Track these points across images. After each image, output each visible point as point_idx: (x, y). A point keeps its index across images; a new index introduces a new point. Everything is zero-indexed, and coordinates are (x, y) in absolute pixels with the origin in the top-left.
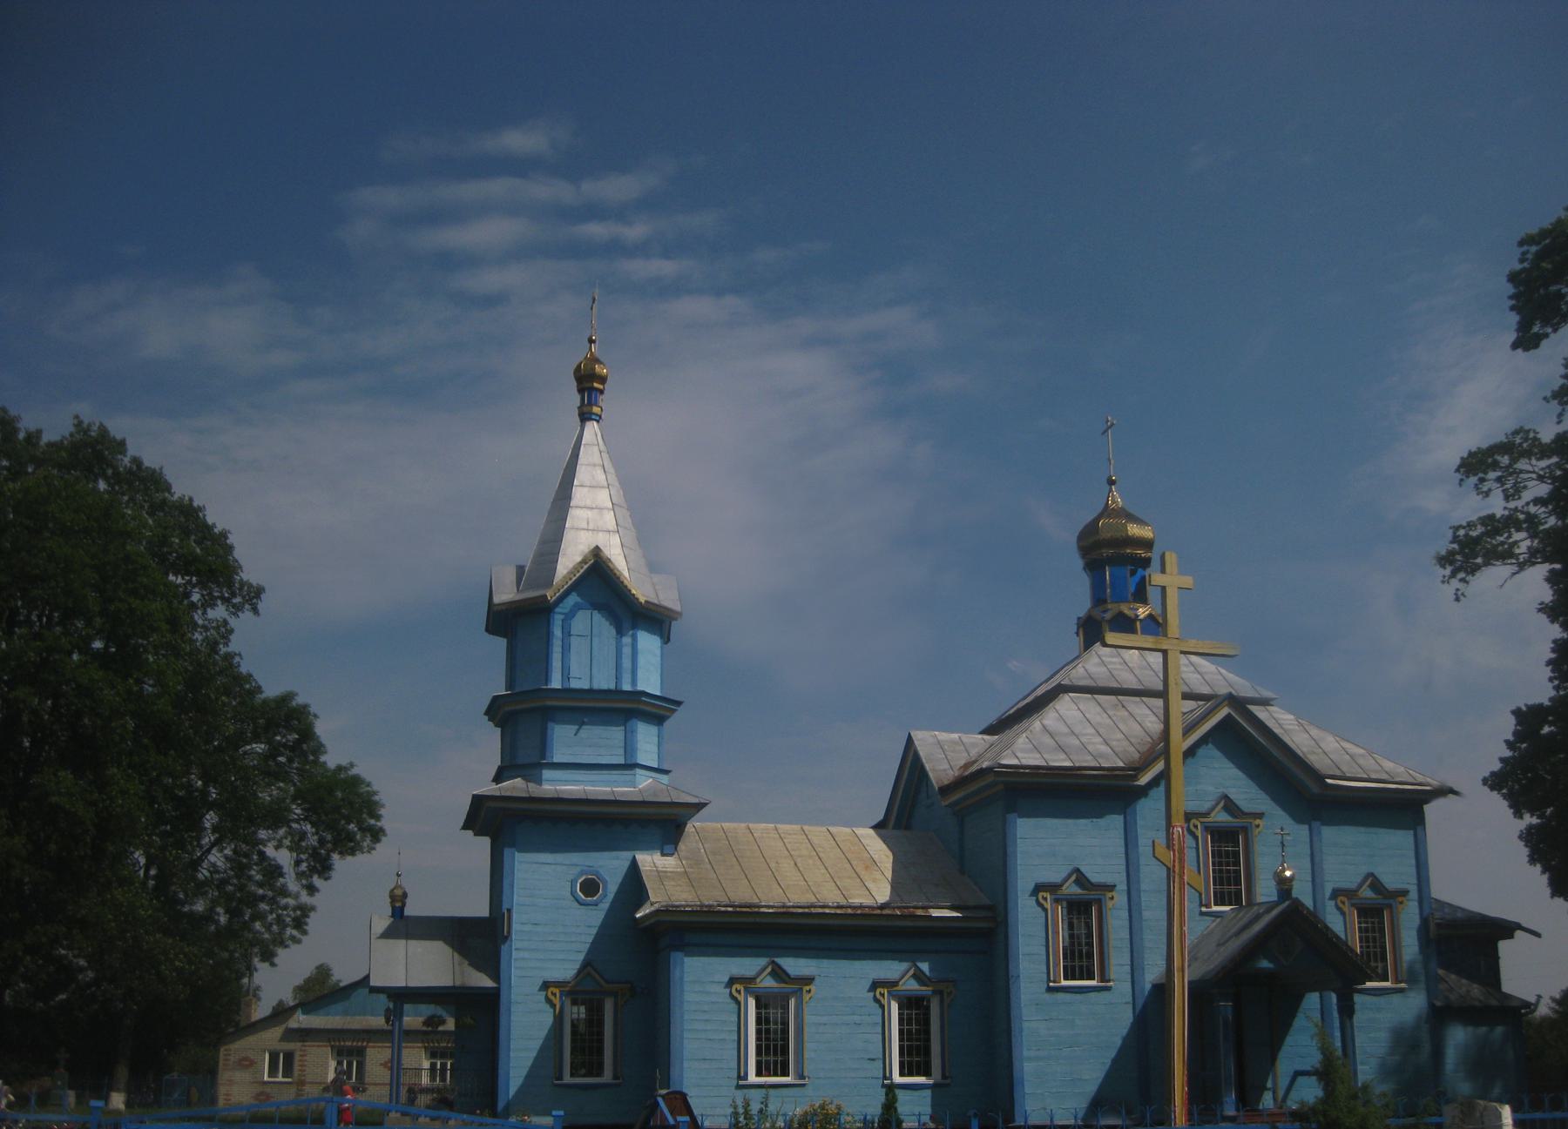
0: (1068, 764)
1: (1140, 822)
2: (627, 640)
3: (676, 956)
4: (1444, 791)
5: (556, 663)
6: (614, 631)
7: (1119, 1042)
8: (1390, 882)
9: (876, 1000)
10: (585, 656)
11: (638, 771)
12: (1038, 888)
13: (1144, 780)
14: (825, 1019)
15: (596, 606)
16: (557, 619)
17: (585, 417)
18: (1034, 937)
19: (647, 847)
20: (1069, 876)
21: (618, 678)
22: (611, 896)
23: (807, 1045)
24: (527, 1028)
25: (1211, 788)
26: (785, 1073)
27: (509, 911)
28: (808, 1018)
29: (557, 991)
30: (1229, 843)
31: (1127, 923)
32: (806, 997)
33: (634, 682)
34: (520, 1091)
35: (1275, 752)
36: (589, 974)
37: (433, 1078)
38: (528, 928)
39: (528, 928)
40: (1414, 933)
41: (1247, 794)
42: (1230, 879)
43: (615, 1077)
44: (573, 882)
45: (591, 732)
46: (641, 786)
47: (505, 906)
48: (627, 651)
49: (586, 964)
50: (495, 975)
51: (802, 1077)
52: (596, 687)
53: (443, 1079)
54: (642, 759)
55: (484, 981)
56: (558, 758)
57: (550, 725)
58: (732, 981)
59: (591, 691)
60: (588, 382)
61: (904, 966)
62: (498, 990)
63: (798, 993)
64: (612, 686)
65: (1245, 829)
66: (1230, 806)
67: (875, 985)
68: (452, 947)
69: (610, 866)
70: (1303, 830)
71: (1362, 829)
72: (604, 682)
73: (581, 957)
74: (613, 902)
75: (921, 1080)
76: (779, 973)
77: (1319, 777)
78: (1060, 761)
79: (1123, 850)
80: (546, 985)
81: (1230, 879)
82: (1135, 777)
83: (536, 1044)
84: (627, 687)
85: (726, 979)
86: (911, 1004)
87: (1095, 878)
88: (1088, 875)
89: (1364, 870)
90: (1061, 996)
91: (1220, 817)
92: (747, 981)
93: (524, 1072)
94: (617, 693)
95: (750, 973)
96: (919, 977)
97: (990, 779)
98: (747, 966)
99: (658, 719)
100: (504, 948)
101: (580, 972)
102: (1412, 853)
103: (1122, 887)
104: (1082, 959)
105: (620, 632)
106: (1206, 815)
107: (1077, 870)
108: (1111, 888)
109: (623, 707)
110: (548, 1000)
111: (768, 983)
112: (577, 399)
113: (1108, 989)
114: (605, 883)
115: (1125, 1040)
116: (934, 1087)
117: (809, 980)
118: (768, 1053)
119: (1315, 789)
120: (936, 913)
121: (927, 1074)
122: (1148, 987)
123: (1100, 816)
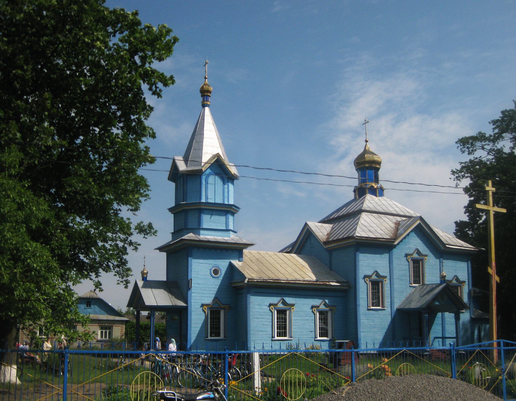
0: (374, 237)
1: (394, 257)
2: (226, 186)
3: (248, 295)
4: (247, 245)
5: (203, 194)
6: (222, 183)
7: (387, 327)
8: (461, 279)
9: (313, 312)
10: (213, 191)
11: (231, 232)
12: (365, 277)
13: (396, 243)
14: (298, 318)
15: (216, 174)
16: (204, 177)
17: (204, 106)
18: (363, 291)
19: (234, 259)
20: (374, 273)
21: (224, 200)
22: (223, 275)
23: (293, 327)
24: (197, 320)
25: (413, 246)
26: (285, 336)
27: (191, 279)
28: (293, 318)
29: (206, 307)
30: (417, 265)
31: (389, 289)
32: (292, 311)
33: (228, 202)
34: (193, 342)
35: (432, 236)
36: (217, 302)
37: (102, 337)
38: (196, 285)
39: (196, 285)
40: (467, 295)
41: (424, 249)
42: (417, 274)
43: (225, 337)
44: (210, 270)
45: (215, 218)
46: (230, 238)
47: (189, 278)
48: (226, 190)
49: (216, 298)
50: (186, 301)
51: (291, 337)
52: (216, 202)
53: (106, 337)
54: (231, 227)
55: (181, 304)
56: (204, 226)
57: (202, 215)
58: (270, 305)
59: (215, 204)
60: (205, 93)
61: (321, 301)
62: (187, 307)
63: (290, 309)
64: (222, 202)
65: (422, 260)
66: (419, 253)
67: (312, 307)
68: (166, 290)
69: (223, 264)
70: (438, 261)
71: (454, 261)
72: (219, 201)
73: (214, 296)
74: (223, 277)
75: (325, 338)
76: (284, 303)
77: (444, 245)
78: (372, 236)
79: (388, 265)
80: (203, 305)
81: (417, 274)
82: (394, 242)
83: (200, 326)
84: (226, 203)
85: (268, 304)
86: (321, 313)
87: (381, 274)
88: (379, 273)
89: (454, 274)
90: (371, 312)
91: (415, 256)
92: (275, 305)
93: (196, 335)
94: (223, 205)
95: (276, 302)
96: (325, 305)
97: (351, 241)
98: (275, 300)
99: (233, 214)
100: (189, 292)
101: (213, 301)
102: (466, 270)
103: (388, 277)
104: (377, 298)
105: (224, 183)
106: (412, 255)
107: (377, 271)
108: (386, 277)
109: (227, 210)
110: (203, 311)
111: (281, 306)
112: (201, 99)
113: (384, 310)
114: (221, 272)
115: (389, 326)
116: (329, 341)
117: (293, 305)
118: (213, 329)
119: (442, 248)
120: (333, 284)
121: (327, 336)
122: (395, 309)
123: (382, 254)
